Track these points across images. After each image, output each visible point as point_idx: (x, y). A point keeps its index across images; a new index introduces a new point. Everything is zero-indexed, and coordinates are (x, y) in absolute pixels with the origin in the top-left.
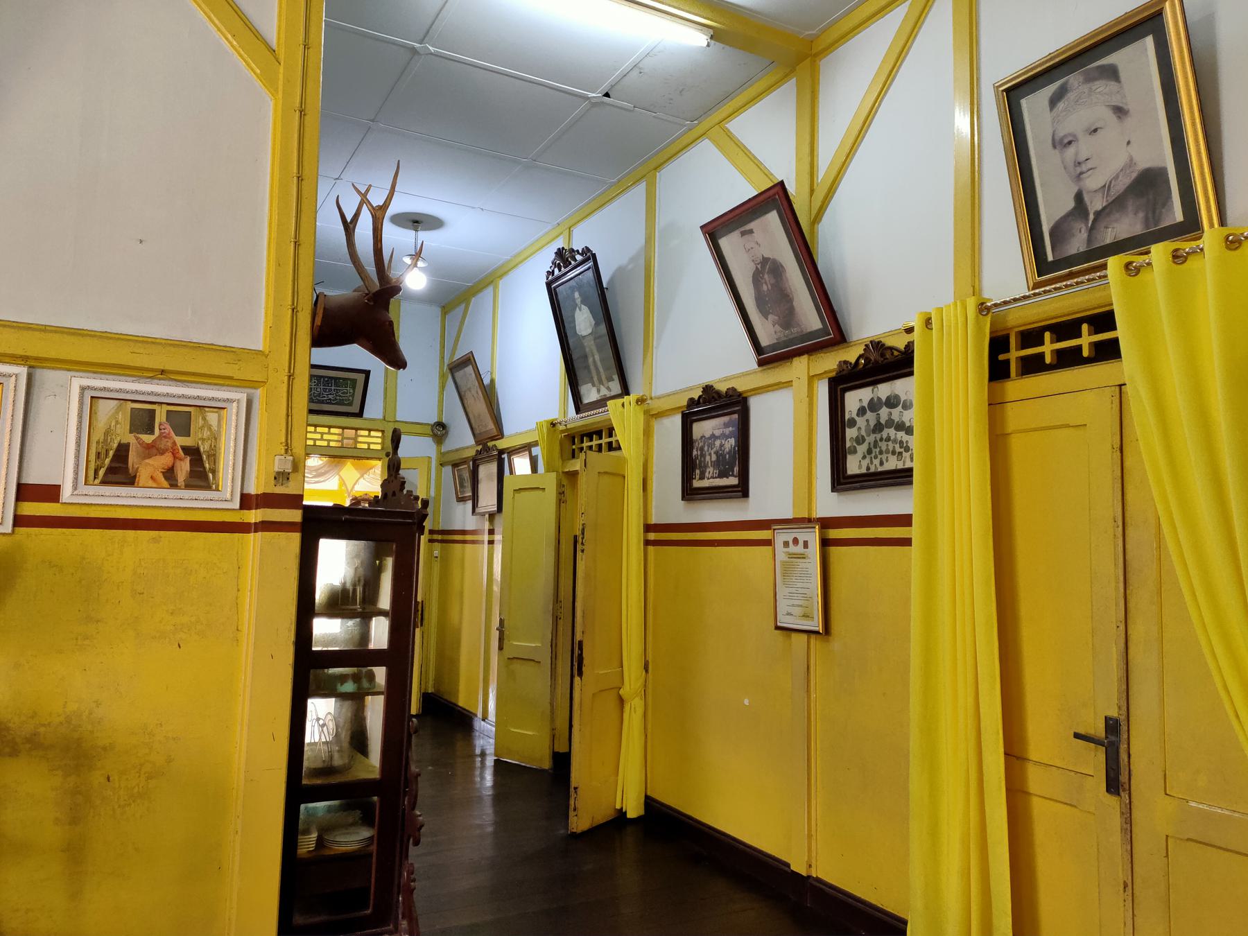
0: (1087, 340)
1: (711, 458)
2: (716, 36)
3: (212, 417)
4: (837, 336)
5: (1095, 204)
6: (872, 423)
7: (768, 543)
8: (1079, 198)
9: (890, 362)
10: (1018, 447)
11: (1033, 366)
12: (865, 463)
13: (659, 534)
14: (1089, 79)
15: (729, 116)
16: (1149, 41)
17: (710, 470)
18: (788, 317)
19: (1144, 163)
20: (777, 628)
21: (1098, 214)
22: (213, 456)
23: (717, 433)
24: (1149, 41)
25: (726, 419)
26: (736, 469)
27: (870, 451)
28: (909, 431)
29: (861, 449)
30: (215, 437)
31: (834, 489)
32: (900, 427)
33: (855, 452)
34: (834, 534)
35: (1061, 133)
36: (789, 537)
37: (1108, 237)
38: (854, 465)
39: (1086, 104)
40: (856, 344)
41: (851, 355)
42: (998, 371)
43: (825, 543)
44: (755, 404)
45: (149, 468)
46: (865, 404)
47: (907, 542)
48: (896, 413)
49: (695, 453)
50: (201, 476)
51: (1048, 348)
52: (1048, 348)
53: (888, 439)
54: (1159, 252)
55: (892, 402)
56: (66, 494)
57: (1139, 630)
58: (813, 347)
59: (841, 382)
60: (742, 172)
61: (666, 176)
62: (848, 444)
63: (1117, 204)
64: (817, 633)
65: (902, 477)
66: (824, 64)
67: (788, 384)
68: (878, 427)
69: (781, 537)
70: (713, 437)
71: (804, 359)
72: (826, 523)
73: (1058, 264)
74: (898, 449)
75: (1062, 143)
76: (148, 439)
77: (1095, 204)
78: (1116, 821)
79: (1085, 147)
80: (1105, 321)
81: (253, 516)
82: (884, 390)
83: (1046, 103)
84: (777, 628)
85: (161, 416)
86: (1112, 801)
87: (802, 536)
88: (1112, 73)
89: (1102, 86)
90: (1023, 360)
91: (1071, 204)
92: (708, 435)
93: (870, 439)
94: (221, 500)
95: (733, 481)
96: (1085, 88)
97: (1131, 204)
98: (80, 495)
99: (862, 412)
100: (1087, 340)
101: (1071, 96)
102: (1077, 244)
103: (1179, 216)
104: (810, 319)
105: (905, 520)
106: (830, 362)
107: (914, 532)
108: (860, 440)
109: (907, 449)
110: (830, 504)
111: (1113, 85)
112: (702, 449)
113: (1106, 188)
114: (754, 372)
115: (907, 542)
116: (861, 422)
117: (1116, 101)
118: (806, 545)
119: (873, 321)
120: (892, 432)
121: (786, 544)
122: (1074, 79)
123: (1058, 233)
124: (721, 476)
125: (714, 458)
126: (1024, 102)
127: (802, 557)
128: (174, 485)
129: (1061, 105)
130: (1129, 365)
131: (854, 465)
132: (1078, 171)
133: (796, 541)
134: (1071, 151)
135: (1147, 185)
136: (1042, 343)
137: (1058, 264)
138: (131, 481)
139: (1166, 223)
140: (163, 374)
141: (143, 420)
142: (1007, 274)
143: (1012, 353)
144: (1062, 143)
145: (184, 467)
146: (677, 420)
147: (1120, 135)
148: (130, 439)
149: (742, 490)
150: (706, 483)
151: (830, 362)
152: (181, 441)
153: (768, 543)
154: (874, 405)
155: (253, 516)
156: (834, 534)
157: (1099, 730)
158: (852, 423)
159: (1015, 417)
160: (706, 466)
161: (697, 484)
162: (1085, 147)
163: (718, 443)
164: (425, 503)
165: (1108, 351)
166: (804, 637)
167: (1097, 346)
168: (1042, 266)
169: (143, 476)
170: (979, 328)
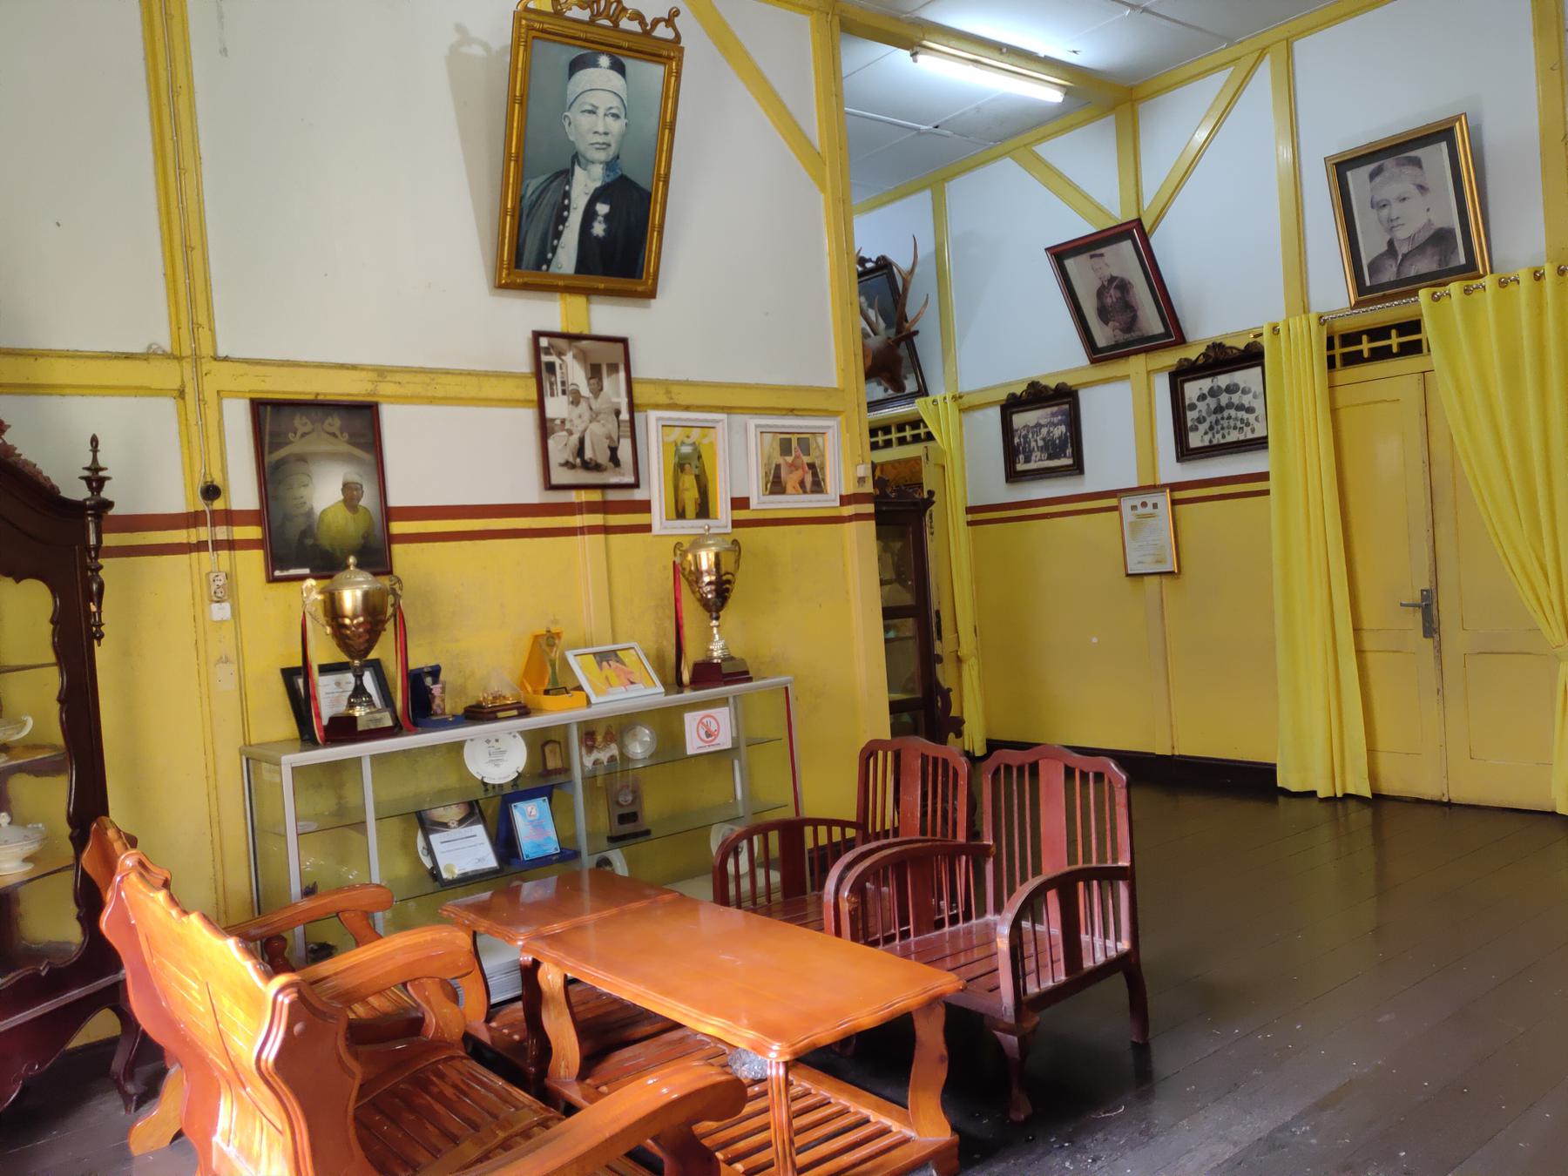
0: (1408, 339)
1: (1037, 442)
2: (1068, 92)
3: (820, 440)
4: (1174, 334)
5: (1403, 249)
6: (1213, 407)
7: (1115, 508)
8: (1391, 243)
9: (1221, 359)
10: (1344, 415)
11: (1353, 359)
12: (1207, 438)
13: (980, 515)
14: (1400, 164)
15: (1039, 141)
16: (1444, 145)
17: (1036, 455)
18: (1131, 323)
19: (1439, 223)
20: (1128, 575)
21: (1405, 256)
22: (823, 469)
23: (1043, 422)
24: (1444, 145)
25: (1055, 409)
26: (1069, 451)
27: (1211, 428)
28: (1250, 410)
29: (1203, 427)
30: (823, 455)
31: (1178, 460)
32: (1240, 408)
33: (1196, 429)
34: (1179, 495)
35: (1377, 198)
36: (1137, 501)
37: (1413, 270)
38: (1195, 440)
39: (1397, 181)
40: (1196, 343)
41: (1193, 353)
42: (1331, 363)
43: (1174, 502)
44: (1085, 397)
45: (791, 480)
46: (1206, 391)
47: (1266, 492)
48: (1236, 398)
49: (1016, 440)
50: (818, 487)
51: (1365, 346)
52: (1365, 346)
53: (1229, 418)
54: (1455, 288)
55: (1232, 389)
56: (753, 504)
57: (1441, 532)
58: (1149, 345)
59: (1180, 376)
60: (1069, 204)
61: (957, 189)
62: (1189, 424)
63: (1419, 250)
64: (1172, 573)
65: (1260, 444)
66: (1142, 108)
67: (1127, 377)
68: (1219, 409)
69: (1126, 503)
70: (1039, 426)
71: (1142, 357)
72: (1174, 487)
73: (1372, 289)
74: (1239, 424)
75: (1379, 205)
76: (789, 459)
77: (1403, 249)
78: (1431, 652)
79: (1396, 210)
80: (1414, 326)
81: (848, 510)
82: (1223, 380)
83: (1366, 176)
84: (1128, 575)
85: (794, 444)
86: (1429, 642)
87: (1150, 499)
88: (1417, 163)
89: (1409, 170)
90: (1344, 355)
91: (1385, 248)
92: (1032, 424)
93: (1213, 418)
94: (828, 502)
95: (1068, 461)
96: (1396, 170)
97: (1429, 251)
98: (762, 504)
99: (1202, 397)
100: (1408, 339)
101: (1386, 174)
102: (1389, 274)
103: (1463, 261)
104: (1152, 323)
105: (1264, 476)
106: (1171, 358)
107: (1271, 485)
108: (1201, 420)
109: (1248, 424)
110: (1171, 470)
111: (1416, 170)
112: (1025, 437)
113: (1411, 239)
114: (1083, 368)
115: (1266, 492)
116: (1201, 406)
117: (1419, 181)
118: (1155, 506)
119: (1209, 324)
120: (1233, 412)
121: (1134, 508)
122: (1389, 163)
123: (1375, 266)
124: (1050, 457)
125: (1041, 443)
126: (1349, 174)
127: (1151, 516)
128: (805, 492)
129: (1378, 179)
130: (1436, 357)
131: (1195, 440)
132: (1391, 225)
133: (1144, 504)
134: (1385, 212)
135: (1441, 238)
136: (1360, 343)
137: (1372, 289)
138: (783, 491)
139: (1452, 265)
140: (791, 412)
141: (785, 447)
142: (1333, 291)
143: (1347, 349)
144: (1379, 205)
145: (809, 479)
146: (995, 414)
147: (1421, 205)
148: (780, 460)
149: (1077, 468)
150: (1032, 466)
151: (1171, 358)
152: (806, 459)
153: (1115, 508)
154: (1214, 393)
155: (848, 510)
156: (1179, 495)
157: (1417, 598)
158: (1193, 407)
159: (1343, 396)
160: (1031, 451)
161: (1020, 467)
162: (1396, 210)
163: (1044, 431)
164: (931, 493)
165: (1414, 348)
166: (1156, 579)
167: (1401, 345)
168: (1361, 288)
169: (789, 488)
170: (1319, 333)
